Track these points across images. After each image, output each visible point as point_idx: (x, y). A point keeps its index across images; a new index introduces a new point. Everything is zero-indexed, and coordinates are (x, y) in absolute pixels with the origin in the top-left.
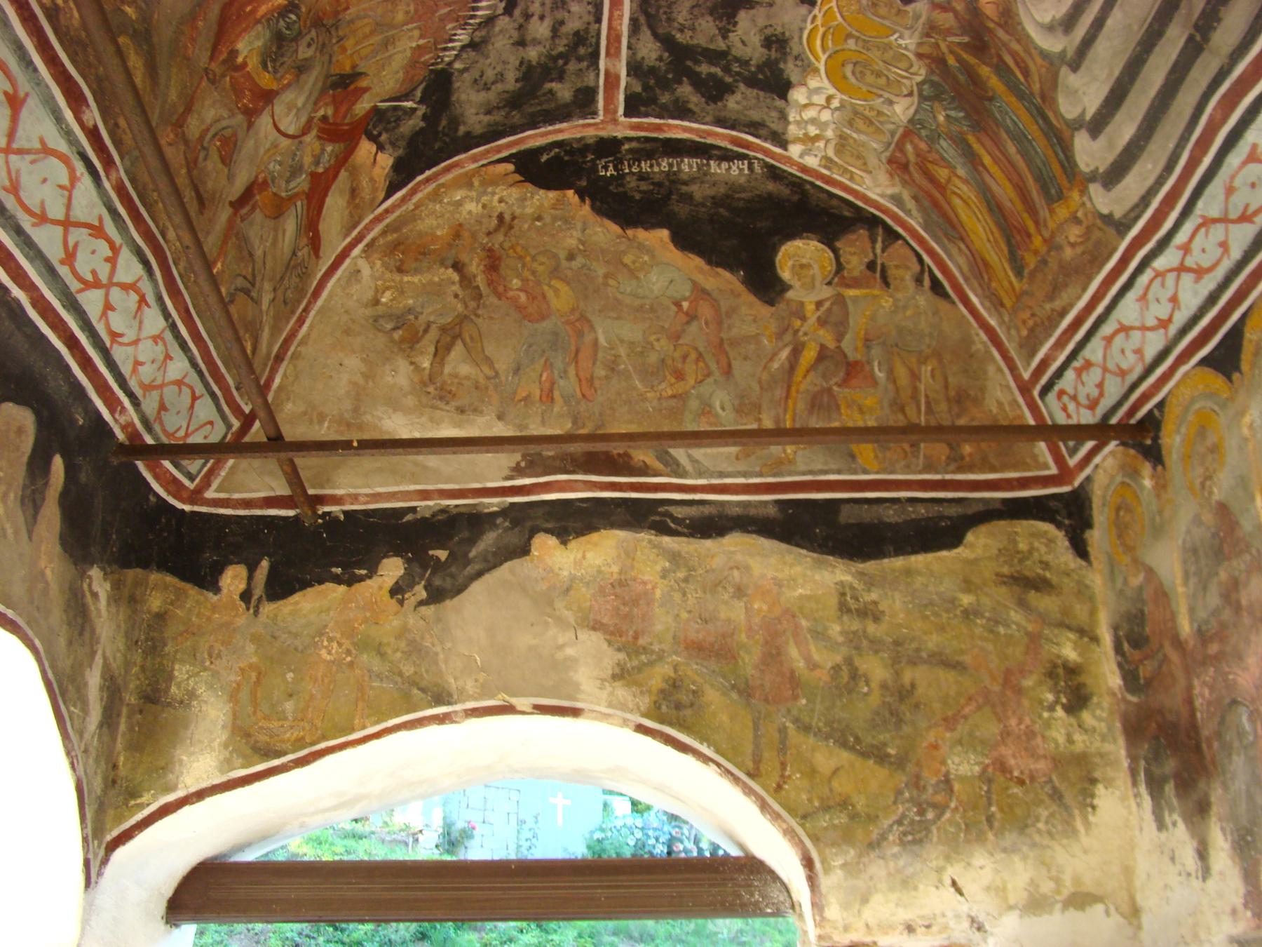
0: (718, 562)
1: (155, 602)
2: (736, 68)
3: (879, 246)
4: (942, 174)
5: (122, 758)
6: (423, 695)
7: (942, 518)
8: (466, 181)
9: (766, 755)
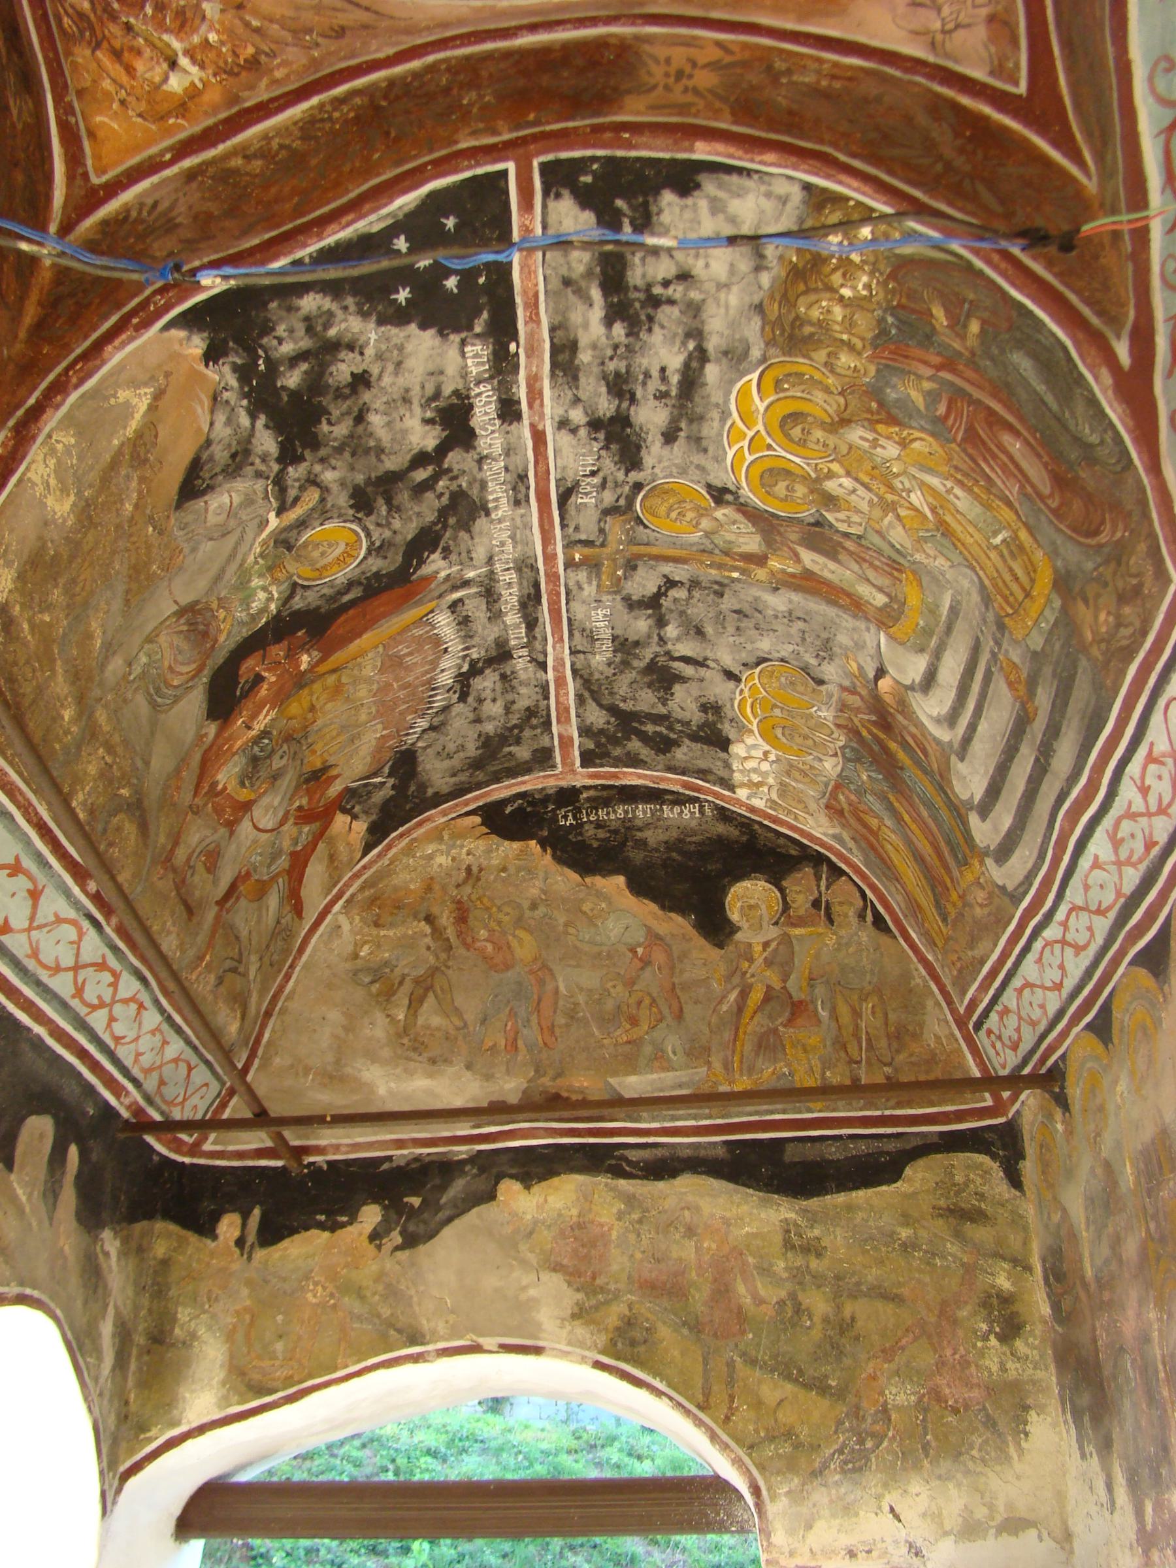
0: (670, 1203)
1: (160, 1249)
2: (678, 727)
3: (823, 883)
4: (874, 823)
5: (132, 1395)
6: (399, 1336)
7: (882, 1153)
8: (437, 835)
9: (715, 1388)
